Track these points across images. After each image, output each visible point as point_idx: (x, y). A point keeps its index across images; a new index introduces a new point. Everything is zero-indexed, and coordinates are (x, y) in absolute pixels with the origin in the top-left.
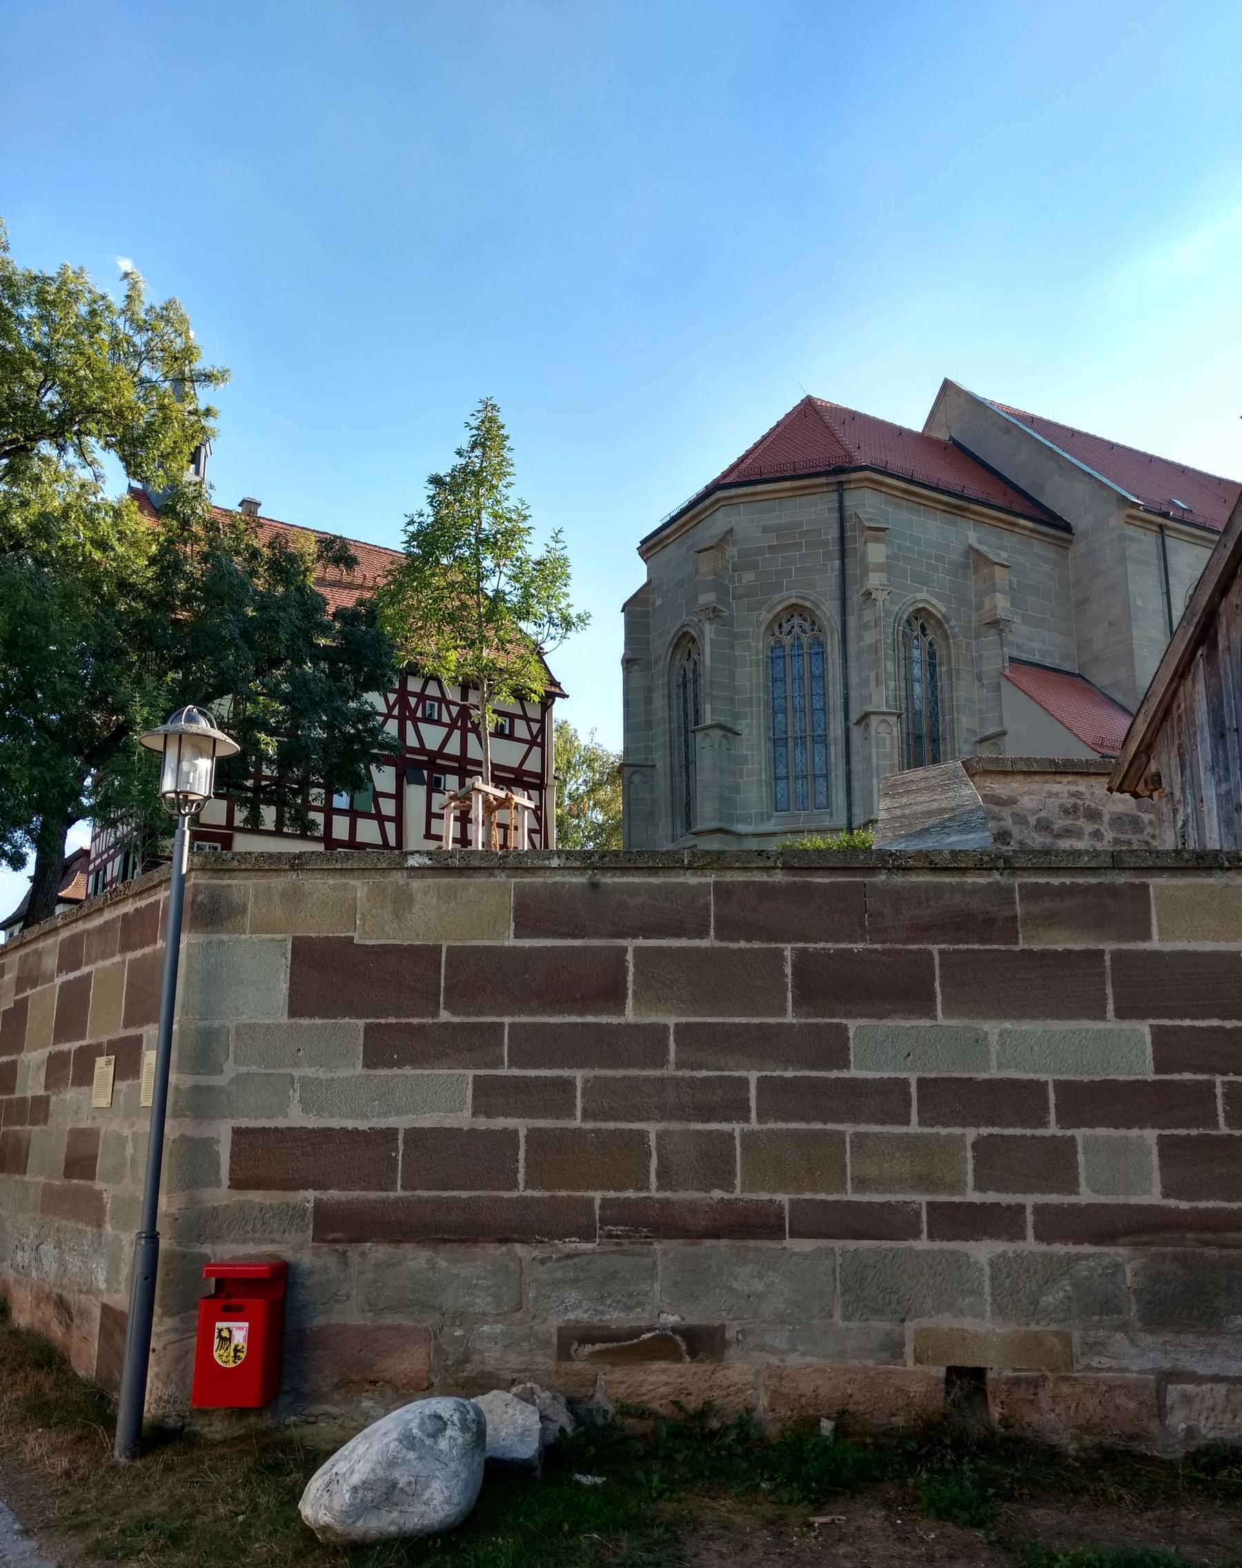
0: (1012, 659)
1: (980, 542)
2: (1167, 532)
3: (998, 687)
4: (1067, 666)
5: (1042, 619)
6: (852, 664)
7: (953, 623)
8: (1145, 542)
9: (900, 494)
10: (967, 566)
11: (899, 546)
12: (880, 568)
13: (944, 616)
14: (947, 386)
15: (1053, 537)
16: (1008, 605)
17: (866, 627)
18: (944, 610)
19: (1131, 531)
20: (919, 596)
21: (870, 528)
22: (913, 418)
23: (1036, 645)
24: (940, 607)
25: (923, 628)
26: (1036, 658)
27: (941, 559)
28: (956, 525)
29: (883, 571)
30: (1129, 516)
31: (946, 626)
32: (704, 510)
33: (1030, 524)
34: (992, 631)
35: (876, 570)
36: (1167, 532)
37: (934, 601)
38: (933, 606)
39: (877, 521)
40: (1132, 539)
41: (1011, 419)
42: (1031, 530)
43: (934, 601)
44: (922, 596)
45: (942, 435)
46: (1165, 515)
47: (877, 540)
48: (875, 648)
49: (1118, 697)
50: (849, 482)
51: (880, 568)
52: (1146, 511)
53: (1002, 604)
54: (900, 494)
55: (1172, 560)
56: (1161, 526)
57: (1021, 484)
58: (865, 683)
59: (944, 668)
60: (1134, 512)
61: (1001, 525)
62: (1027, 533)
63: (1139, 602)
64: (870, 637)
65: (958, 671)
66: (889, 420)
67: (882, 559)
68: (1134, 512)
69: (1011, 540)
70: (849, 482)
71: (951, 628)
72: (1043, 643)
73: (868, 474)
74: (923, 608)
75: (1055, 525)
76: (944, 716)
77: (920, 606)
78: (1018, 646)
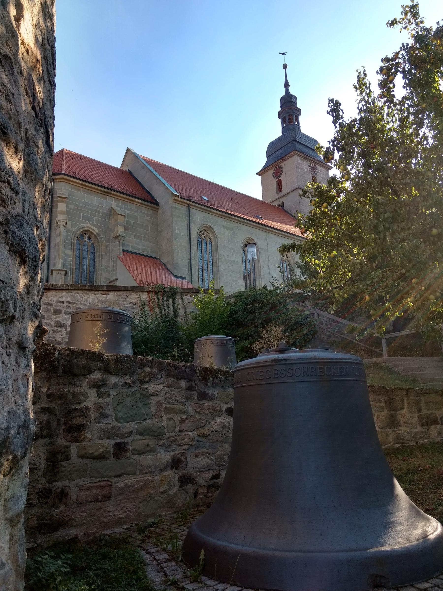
0: (123, 250)
1: (117, 206)
2: (190, 206)
3: (116, 262)
4: (154, 255)
5: (144, 237)
6: (52, 250)
7: (101, 236)
8: (183, 209)
9: (79, 186)
10: (110, 215)
11: (78, 206)
12: (62, 213)
13: (97, 234)
14: (128, 150)
15: (150, 206)
16: (124, 230)
17: (56, 236)
18: (97, 231)
19: (176, 205)
20: (85, 225)
21: (59, 197)
22: (117, 163)
23: (140, 247)
24: (95, 230)
25: (89, 238)
26: (140, 252)
27: (98, 212)
28: (106, 199)
29: (64, 214)
30: (174, 200)
31: (98, 238)
32: (250, 224)
33: (140, 201)
34: (117, 240)
35: (61, 214)
36: (190, 206)
37: (93, 227)
38: (93, 229)
39: (65, 195)
40: (176, 208)
41: (143, 161)
42: (141, 203)
43: (93, 227)
44: (87, 225)
45: (125, 169)
46: (190, 200)
47: (62, 202)
48: (59, 244)
49: (169, 267)
50: (56, 179)
51: (62, 213)
52: (181, 198)
53: (120, 230)
54: (79, 186)
55: (193, 217)
56: (188, 204)
57: (146, 187)
58: (55, 258)
59: (98, 254)
60: (176, 198)
61: (127, 200)
62: (139, 204)
63: (177, 232)
64: (58, 240)
65: (102, 255)
66: (97, 159)
67: (64, 209)
68: (176, 198)
69: (131, 206)
70: (56, 179)
71: (100, 238)
72: (144, 246)
73: (63, 176)
74: (88, 230)
75: (153, 202)
76: (96, 272)
77: (86, 229)
78: (132, 247)
